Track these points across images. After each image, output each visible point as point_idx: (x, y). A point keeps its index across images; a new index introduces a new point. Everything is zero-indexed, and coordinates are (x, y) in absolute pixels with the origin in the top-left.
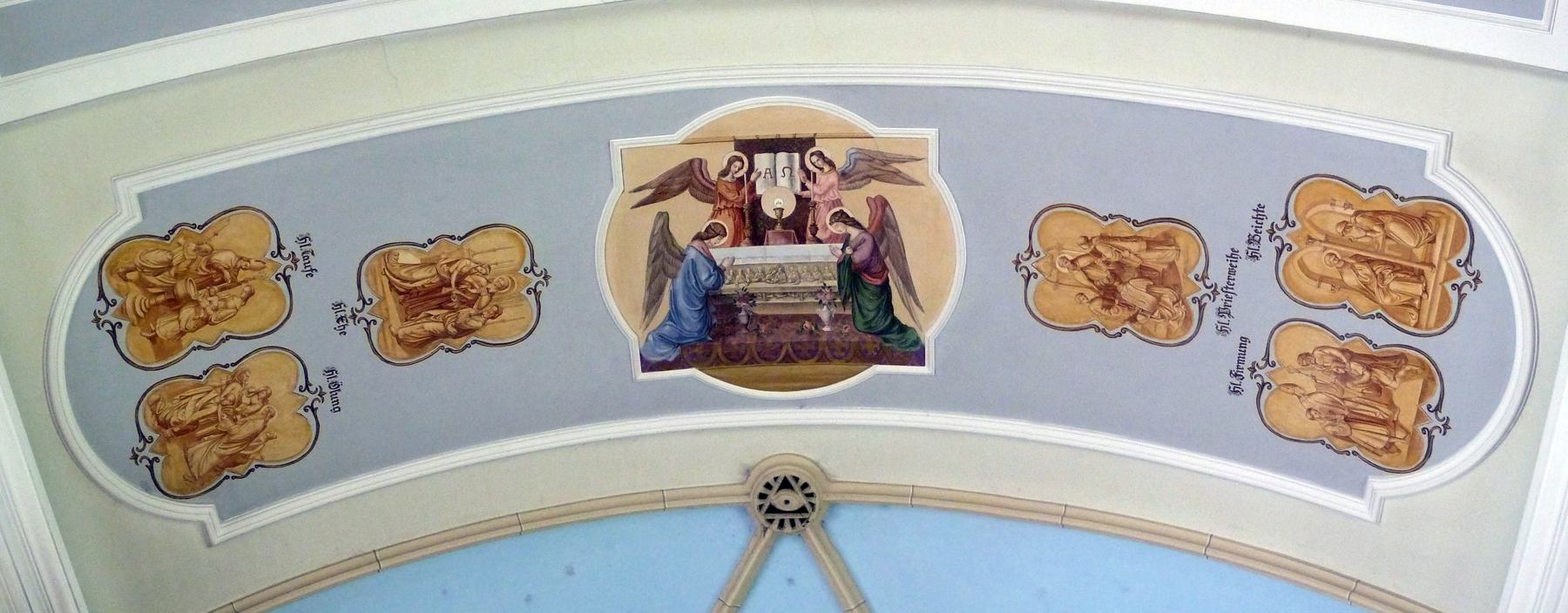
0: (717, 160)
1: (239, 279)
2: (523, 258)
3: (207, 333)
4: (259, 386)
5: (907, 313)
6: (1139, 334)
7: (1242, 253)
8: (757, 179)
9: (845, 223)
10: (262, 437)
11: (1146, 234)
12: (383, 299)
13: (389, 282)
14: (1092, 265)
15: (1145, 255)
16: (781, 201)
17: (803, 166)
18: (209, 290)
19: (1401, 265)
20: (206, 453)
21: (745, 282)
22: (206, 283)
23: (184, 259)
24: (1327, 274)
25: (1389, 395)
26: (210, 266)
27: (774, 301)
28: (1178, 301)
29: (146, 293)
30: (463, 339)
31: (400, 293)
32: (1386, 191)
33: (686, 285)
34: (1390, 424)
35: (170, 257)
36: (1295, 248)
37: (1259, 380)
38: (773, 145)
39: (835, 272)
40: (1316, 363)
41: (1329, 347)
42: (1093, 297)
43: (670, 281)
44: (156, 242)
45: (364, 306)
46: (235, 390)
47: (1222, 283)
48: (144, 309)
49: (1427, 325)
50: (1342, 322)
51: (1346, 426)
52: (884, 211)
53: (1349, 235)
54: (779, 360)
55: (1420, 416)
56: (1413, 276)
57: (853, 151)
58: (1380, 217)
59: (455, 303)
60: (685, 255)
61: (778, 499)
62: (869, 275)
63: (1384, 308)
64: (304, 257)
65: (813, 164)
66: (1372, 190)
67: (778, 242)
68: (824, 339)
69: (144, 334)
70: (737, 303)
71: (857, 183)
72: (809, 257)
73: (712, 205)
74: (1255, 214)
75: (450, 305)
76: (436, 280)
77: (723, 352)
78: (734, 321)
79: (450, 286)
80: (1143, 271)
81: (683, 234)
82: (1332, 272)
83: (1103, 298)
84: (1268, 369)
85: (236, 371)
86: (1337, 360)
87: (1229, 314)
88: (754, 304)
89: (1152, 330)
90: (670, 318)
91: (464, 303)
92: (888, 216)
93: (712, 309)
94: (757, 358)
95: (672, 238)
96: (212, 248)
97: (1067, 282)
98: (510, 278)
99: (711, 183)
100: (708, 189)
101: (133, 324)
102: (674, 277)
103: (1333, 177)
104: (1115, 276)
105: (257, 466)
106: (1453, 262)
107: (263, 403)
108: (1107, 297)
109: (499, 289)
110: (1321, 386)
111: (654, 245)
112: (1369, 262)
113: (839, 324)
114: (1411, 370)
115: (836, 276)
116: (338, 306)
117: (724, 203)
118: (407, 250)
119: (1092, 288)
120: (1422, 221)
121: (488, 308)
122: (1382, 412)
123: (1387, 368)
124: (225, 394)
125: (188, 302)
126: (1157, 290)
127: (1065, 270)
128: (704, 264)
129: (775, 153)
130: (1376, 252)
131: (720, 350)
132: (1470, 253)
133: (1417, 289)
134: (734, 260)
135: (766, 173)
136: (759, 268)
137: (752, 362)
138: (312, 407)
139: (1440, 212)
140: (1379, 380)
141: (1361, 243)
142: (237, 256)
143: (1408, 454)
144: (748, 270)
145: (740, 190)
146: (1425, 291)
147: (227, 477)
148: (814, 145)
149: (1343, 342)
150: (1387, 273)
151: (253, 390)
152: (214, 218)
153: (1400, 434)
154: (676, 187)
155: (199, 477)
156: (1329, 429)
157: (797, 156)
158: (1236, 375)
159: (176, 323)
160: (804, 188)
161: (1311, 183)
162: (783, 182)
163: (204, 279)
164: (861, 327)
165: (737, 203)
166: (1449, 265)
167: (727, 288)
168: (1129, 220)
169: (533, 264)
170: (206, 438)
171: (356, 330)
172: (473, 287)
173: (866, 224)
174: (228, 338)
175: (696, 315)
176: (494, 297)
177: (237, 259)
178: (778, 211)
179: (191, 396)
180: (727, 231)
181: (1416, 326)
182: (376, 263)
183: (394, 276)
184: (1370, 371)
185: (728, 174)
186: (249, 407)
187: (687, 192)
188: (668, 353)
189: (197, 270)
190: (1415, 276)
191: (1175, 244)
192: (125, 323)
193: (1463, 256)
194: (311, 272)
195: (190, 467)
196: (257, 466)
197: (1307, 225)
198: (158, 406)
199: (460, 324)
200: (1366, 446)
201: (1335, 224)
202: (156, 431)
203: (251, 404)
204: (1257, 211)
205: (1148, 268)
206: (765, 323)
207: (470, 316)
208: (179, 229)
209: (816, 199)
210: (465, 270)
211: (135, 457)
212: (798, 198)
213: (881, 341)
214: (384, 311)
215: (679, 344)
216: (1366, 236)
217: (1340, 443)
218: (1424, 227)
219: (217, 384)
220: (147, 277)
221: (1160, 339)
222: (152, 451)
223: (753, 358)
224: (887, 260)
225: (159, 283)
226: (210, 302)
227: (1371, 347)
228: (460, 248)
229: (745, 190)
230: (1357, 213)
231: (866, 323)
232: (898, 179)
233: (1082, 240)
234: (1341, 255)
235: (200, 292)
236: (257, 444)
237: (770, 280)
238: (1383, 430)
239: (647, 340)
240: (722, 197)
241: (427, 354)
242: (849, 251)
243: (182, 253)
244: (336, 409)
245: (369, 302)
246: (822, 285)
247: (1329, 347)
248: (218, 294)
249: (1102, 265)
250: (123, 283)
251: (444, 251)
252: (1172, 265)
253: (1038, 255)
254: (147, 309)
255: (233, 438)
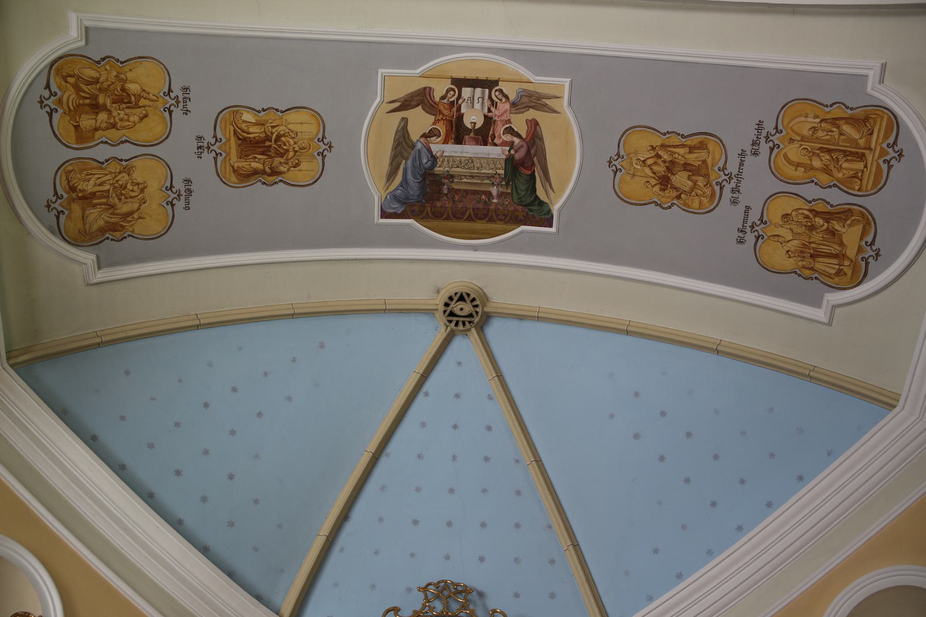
0: (440, 89)
1: (140, 104)
2: (319, 131)
3: (112, 134)
4: (139, 180)
5: (544, 193)
6: (682, 207)
7: (748, 152)
8: (462, 103)
9: (512, 134)
10: (136, 215)
11: (689, 143)
12: (229, 140)
13: (234, 130)
14: (655, 163)
15: (688, 156)
16: (475, 118)
17: (490, 97)
18: (119, 106)
19: (850, 151)
20: (97, 217)
21: (449, 167)
22: (118, 101)
23: (107, 80)
24: (801, 161)
25: (840, 237)
26: (123, 89)
27: (465, 180)
28: (707, 184)
29: (78, 94)
30: (275, 177)
31: (240, 139)
32: (840, 105)
33: (414, 165)
34: (840, 256)
35: (98, 76)
36: (781, 146)
37: (756, 234)
38: (474, 83)
39: (503, 165)
40: (793, 220)
41: (800, 209)
42: (655, 183)
43: (404, 161)
44: (92, 63)
45: (216, 142)
46: (124, 178)
47: (735, 172)
48: (74, 105)
49: (866, 189)
50: (810, 191)
51: (811, 260)
52: (535, 128)
53: (817, 135)
54: (465, 218)
55: (860, 250)
56: (857, 158)
57: (520, 90)
58: (837, 122)
59: (272, 153)
60: (415, 146)
61: (456, 307)
62: (524, 168)
63: (837, 179)
64: (184, 100)
65: (496, 97)
66: (831, 105)
67: (471, 144)
68: (493, 207)
69: (72, 122)
70: (443, 180)
71: (521, 110)
72: (489, 154)
73: (434, 117)
74: (757, 127)
75: (269, 153)
76: (263, 135)
77: (431, 211)
78: (440, 192)
79: (271, 141)
80: (686, 166)
81: (415, 134)
82: (806, 160)
83: (661, 184)
84: (763, 226)
85: (127, 166)
86: (807, 217)
87: (739, 192)
88: (453, 182)
89: (690, 204)
90: (401, 185)
91: (278, 154)
92: (537, 131)
93: (428, 182)
94: (451, 216)
95: (409, 135)
96: (127, 78)
97: (639, 174)
98: (309, 143)
99: (435, 103)
100: (433, 106)
101: (65, 113)
102: (407, 159)
103: (807, 99)
104: (668, 169)
105: (129, 236)
106: (885, 146)
107: (141, 192)
108: (664, 183)
109: (301, 149)
110: (796, 235)
111: (397, 137)
112: (829, 151)
113: (503, 198)
114: (855, 219)
115: (504, 167)
116: (200, 138)
117: (441, 116)
118: (248, 112)
119: (654, 178)
120: (864, 122)
121: (292, 160)
122: (835, 249)
123: (839, 220)
124: (117, 179)
125: (104, 110)
126: (694, 178)
127: (639, 167)
128: (425, 153)
129: (475, 88)
130: (833, 145)
131: (429, 209)
132: (896, 138)
133: (860, 166)
134: (443, 152)
135: (468, 100)
136: (458, 159)
137: (448, 218)
138: (171, 203)
139: (877, 114)
140: (833, 228)
141: (824, 140)
142: (141, 88)
143: (852, 277)
144: (451, 159)
145: (452, 108)
146: (866, 166)
147: (108, 238)
148: (498, 85)
149: (810, 205)
150: (841, 157)
151: (136, 181)
152: (131, 59)
153: (847, 263)
154: (414, 103)
155: (89, 233)
156: (800, 263)
157: (487, 91)
158: (742, 231)
159: (94, 121)
160: (489, 111)
161: (794, 104)
162: (477, 106)
163: (117, 97)
164: (516, 200)
165: (449, 117)
166: (882, 148)
167: (438, 170)
168: (679, 134)
169: (324, 137)
170: (99, 206)
171: (208, 157)
172: (285, 145)
173: (524, 136)
174: (126, 141)
175: (417, 185)
176: (297, 154)
177: (141, 90)
178: (473, 124)
179: (94, 174)
180: (441, 134)
181: (859, 190)
182: (228, 115)
183: (238, 127)
184: (828, 222)
185: (445, 99)
186: (130, 193)
187: (420, 107)
188: (398, 208)
189: (114, 90)
190: (859, 157)
191: (707, 148)
192: (60, 111)
193: (891, 140)
194: (187, 112)
195: (84, 224)
196: (129, 236)
197: (790, 131)
198: (71, 175)
199: (273, 167)
200: (824, 273)
201: (808, 129)
202: (66, 192)
203: (132, 191)
204: (758, 124)
205: (689, 164)
206: (458, 194)
207: (280, 163)
208: (108, 59)
209: (496, 118)
210: (282, 133)
211: (48, 206)
212: (485, 116)
213: (527, 210)
214: (228, 149)
215: (405, 203)
216: (827, 135)
217: (807, 272)
218: (865, 125)
219: (113, 171)
220: (80, 84)
221: (695, 209)
222: (61, 205)
223: (448, 216)
224: (535, 159)
225: (87, 90)
226: (119, 114)
227: (829, 206)
228: (281, 118)
229: (455, 109)
230: (821, 121)
231: (519, 198)
232: (546, 109)
233: (649, 148)
234: (811, 149)
235: (113, 105)
236: (131, 219)
237: (464, 167)
238: (836, 261)
239: (386, 197)
240: (440, 112)
241: (249, 183)
242: (512, 152)
243: (107, 75)
244: (187, 208)
245: (219, 141)
246: (495, 172)
247: (800, 209)
248: (125, 110)
249: (661, 163)
250: (63, 83)
251: (271, 117)
252: (704, 162)
253: (623, 158)
254: (76, 105)
255: (116, 211)
